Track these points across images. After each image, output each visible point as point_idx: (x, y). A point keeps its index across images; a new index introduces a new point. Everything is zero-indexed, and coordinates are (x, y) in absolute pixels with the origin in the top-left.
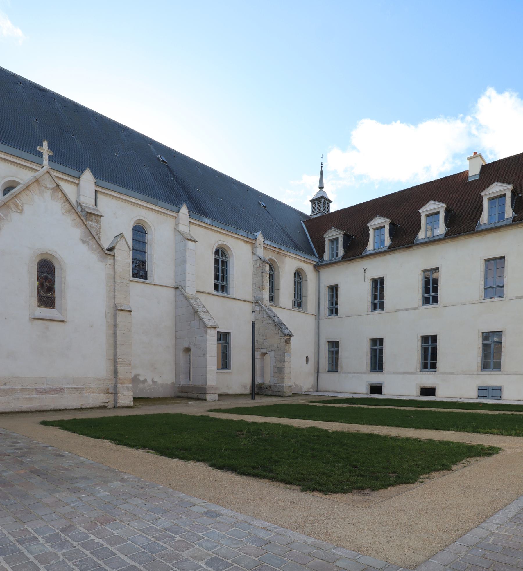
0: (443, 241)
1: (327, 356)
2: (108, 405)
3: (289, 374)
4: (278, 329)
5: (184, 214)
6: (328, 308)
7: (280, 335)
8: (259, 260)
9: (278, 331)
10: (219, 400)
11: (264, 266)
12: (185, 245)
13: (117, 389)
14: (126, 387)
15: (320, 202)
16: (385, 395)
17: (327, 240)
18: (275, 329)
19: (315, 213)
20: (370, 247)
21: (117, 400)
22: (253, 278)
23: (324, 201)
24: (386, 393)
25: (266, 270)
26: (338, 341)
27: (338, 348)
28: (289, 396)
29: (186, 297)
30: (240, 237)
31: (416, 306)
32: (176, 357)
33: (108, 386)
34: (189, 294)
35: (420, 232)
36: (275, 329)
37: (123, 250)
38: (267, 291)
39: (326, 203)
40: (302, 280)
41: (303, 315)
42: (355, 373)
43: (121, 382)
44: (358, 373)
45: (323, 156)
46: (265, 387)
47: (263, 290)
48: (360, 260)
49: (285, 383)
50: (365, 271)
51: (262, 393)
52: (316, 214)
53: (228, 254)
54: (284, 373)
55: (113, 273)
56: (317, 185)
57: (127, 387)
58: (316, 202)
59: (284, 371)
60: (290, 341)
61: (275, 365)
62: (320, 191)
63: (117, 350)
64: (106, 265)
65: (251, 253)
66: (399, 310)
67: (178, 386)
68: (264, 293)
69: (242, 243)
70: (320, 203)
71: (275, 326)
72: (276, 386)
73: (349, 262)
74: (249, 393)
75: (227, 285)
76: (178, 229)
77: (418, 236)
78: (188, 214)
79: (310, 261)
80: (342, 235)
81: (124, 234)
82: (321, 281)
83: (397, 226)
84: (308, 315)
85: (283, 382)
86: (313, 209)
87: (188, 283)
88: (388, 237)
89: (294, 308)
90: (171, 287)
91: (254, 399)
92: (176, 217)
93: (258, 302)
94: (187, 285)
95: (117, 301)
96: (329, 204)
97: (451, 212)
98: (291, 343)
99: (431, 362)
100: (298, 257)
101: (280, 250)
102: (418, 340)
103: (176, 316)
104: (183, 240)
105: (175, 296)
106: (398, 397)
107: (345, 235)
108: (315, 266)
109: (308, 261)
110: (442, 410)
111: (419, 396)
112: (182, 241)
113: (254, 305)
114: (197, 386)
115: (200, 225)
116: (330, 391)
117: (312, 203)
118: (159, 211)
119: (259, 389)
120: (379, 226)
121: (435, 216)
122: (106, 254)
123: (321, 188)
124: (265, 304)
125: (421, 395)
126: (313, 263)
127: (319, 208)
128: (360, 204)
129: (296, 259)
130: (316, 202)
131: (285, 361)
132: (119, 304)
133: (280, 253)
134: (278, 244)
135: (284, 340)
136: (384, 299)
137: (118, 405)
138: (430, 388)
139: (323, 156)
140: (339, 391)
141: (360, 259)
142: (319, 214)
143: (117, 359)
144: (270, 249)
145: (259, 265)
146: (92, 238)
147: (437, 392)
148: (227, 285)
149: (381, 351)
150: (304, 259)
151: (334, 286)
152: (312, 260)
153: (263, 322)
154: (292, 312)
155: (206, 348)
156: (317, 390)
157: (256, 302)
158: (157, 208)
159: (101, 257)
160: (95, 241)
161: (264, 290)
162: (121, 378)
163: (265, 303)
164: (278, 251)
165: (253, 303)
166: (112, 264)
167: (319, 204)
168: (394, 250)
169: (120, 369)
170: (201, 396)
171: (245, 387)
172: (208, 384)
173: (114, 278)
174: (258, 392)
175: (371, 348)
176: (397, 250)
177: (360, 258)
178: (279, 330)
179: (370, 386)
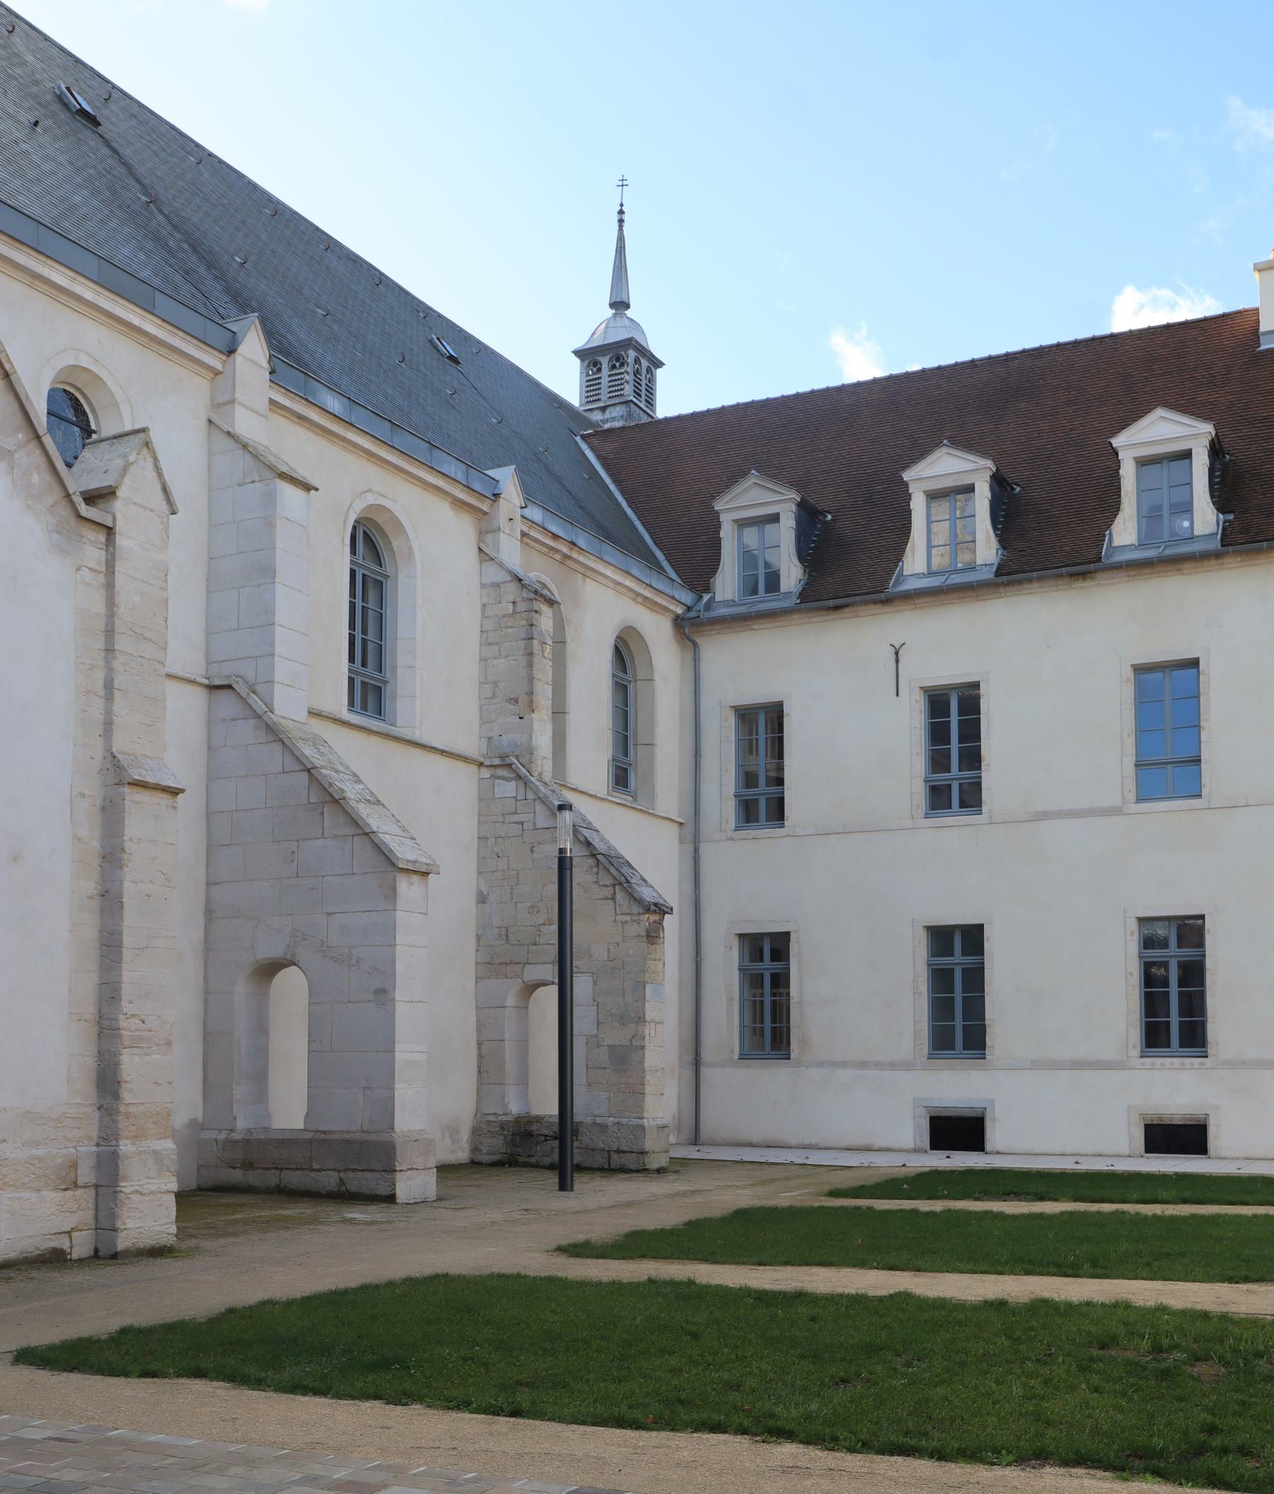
0: (1213, 562)
1: (737, 996)
2: (71, 1248)
3: (659, 1074)
4: (609, 881)
5: (251, 361)
6: (735, 796)
7: (620, 906)
8: (512, 587)
9: (608, 892)
10: (440, 1199)
11: (536, 612)
12: (270, 501)
13: (120, 1163)
14: (155, 1152)
15: (618, 361)
16: (998, 1153)
17: (727, 521)
18: (597, 882)
19: (601, 404)
20: (915, 561)
21: (113, 1216)
22: (483, 660)
23: (637, 361)
24: (1000, 1147)
25: (543, 627)
26: (788, 934)
27: (789, 960)
28: (659, 1171)
29: (275, 734)
30: (441, 483)
31: (1113, 800)
32: (206, 1002)
33: (73, 1150)
34: (282, 717)
35: (1119, 519)
36: (597, 882)
37: (145, 508)
38: (545, 717)
39: (644, 371)
40: (629, 676)
41: (643, 819)
42: (863, 1065)
43: (134, 1128)
44: (879, 1065)
45: (625, 183)
46: (546, 1132)
47: (533, 711)
48: (876, 611)
49: (645, 1115)
50: (897, 654)
51: (533, 1160)
52: (603, 409)
53: (391, 551)
54: (643, 1071)
55: (101, 608)
56: (605, 296)
57: (156, 1153)
58: (605, 361)
59: (642, 1062)
60: (661, 935)
61: (596, 1036)
62: (615, 315)
63: (120, 976)
64: (79, 569)
65: (473, 555)
66: (1042, 816)
67: (222, 1136)
68: (535, 727)
69: (443, 509)
70: (622, 365)
71: (595, 869)
72: (603, 1128)
73: (829, 617)
74: (468, 1161)
75: (385, 682)
76: (226, 428)
77: (1111, 535)
78: (266, 366)
79: (664, 603)
80: (794, 508)
81: (151, 433)
82: (704, 687)
83: (1009, 489)
84: (656, 820)
85: (640, 1107)
86: (587, 392)
87: (282, 670)
88: (987, 531)
89: (614, 794)
90: (192, 682)
91: (572, 1190)
92: (217, 373)
93: (508, 761)
94: (276, 680)
95: (120, 743)
96: (652, 372)
97: (1220, 456)
98: (663, 943)
99: (1180, 1022)
100: (629, 582)
101: (571, 549)
102: (1128, 932)
103: (209, 815)
104: (257, 479)
105: (210, 724)
106: (1077, 1163)
107: (802, 505)
108: (679, 622)
109: (658, 599)
110: (925, 1206)
111: (1142, 1156)
112: (248, 480)
113: (486, 773)
114: (336, 1136)
115: (301, 418)
116: (755, 1140)
117: (582, 361)
118: (154, 339)
119: (518, 1139)
120: (949, 483)
121: (1171, 463)
122: (80, 517)
123: (620, 305)
124: (540, 774)
125: (1147, 1151)
126: (672, 607)
127: (616, 387)
128: (828, 389)
129: (618, 588)
130: (600, 359)
131: (647, 1018)
132: (129, 755)
133: (569, 563)
134: (568, 525)
135: (640, 929)
136: (983, 768)
137: (122, 1243)
138: (1182, 1123)
139: (625, 183)
140: (793, 1143)
141: (877, 606)
142: (618, 408)
143: (121, 1017)
144: (537, 541)
145: (511, 606)
146: (29, 441)
147: (1216, 1140)
148: (385, 682)
149: (976, 979)
150: (647, 593)
151: (761, 708)
152: (673, 598)
153: (532, 851)
154: (606, 806)
155: (393, 962)
156: (695, 1139)
157: (497, 762)
158: (150, 325)
159: (57, 532)
160: (38, 452)
161: (536, 712)
162: (132, 1109)
163: (539, 769)
164: (565, 550)
165: (481, 764)
166: (98, 568)
167: (614, 367)
168: (1020, 582)
169: (131, 1065)
170: (371, 1182)
171: (452, 1131)
172: (399, 1125)
173: (110, 633)
174: (512, 1155)
175: (929, 965)
176: (1030, 580)
177: (875, 602)
178: (614, 886)
179: (932, 1119)
